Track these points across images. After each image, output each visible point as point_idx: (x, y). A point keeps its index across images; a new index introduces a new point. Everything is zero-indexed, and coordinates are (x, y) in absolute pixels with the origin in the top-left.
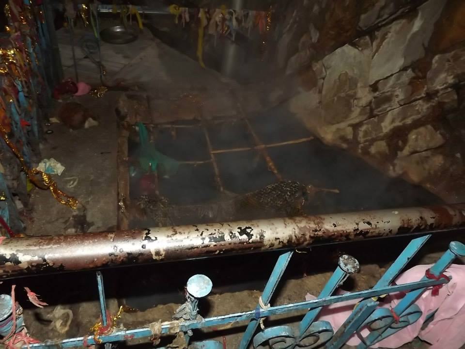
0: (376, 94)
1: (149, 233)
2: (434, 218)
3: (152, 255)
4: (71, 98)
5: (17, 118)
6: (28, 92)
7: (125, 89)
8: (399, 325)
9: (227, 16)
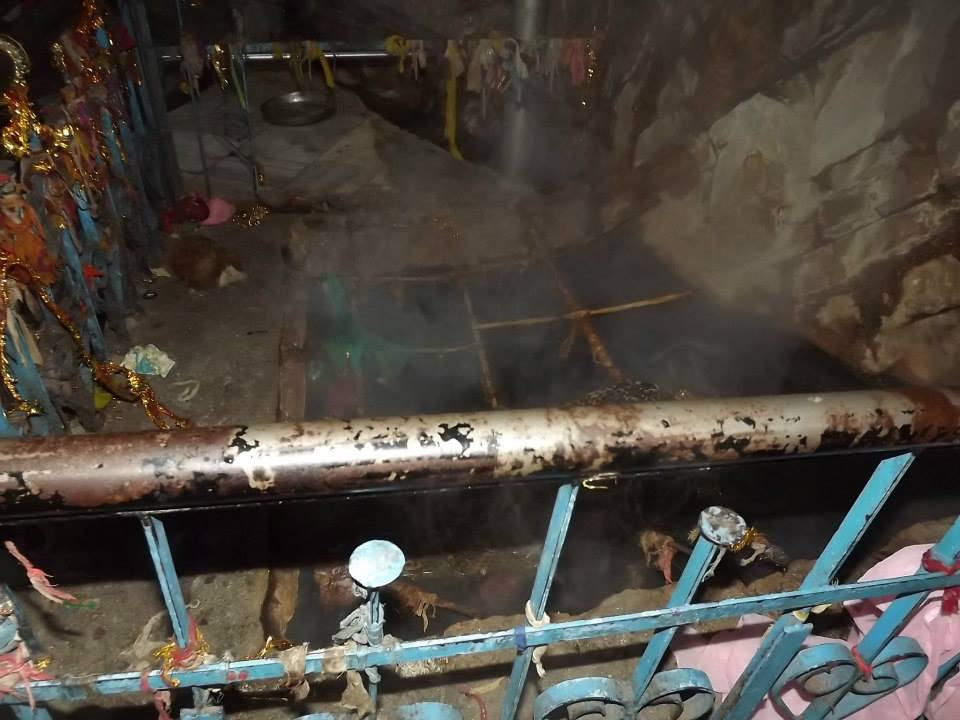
0: (829, 195)
1: (243, 433)
2: (910, 412)
3: (247, 477)
4: (196, 230)
5: (75, 260)
6: (97, 211)
7: (304, 209)
8: (872, 685)
9: (505, 53)
